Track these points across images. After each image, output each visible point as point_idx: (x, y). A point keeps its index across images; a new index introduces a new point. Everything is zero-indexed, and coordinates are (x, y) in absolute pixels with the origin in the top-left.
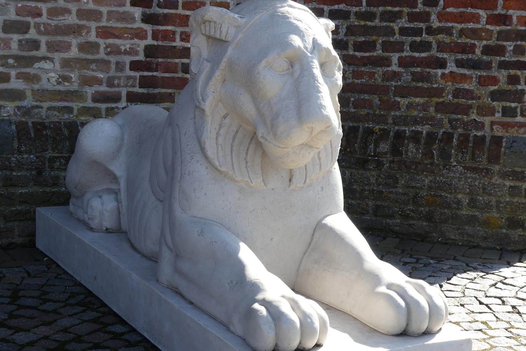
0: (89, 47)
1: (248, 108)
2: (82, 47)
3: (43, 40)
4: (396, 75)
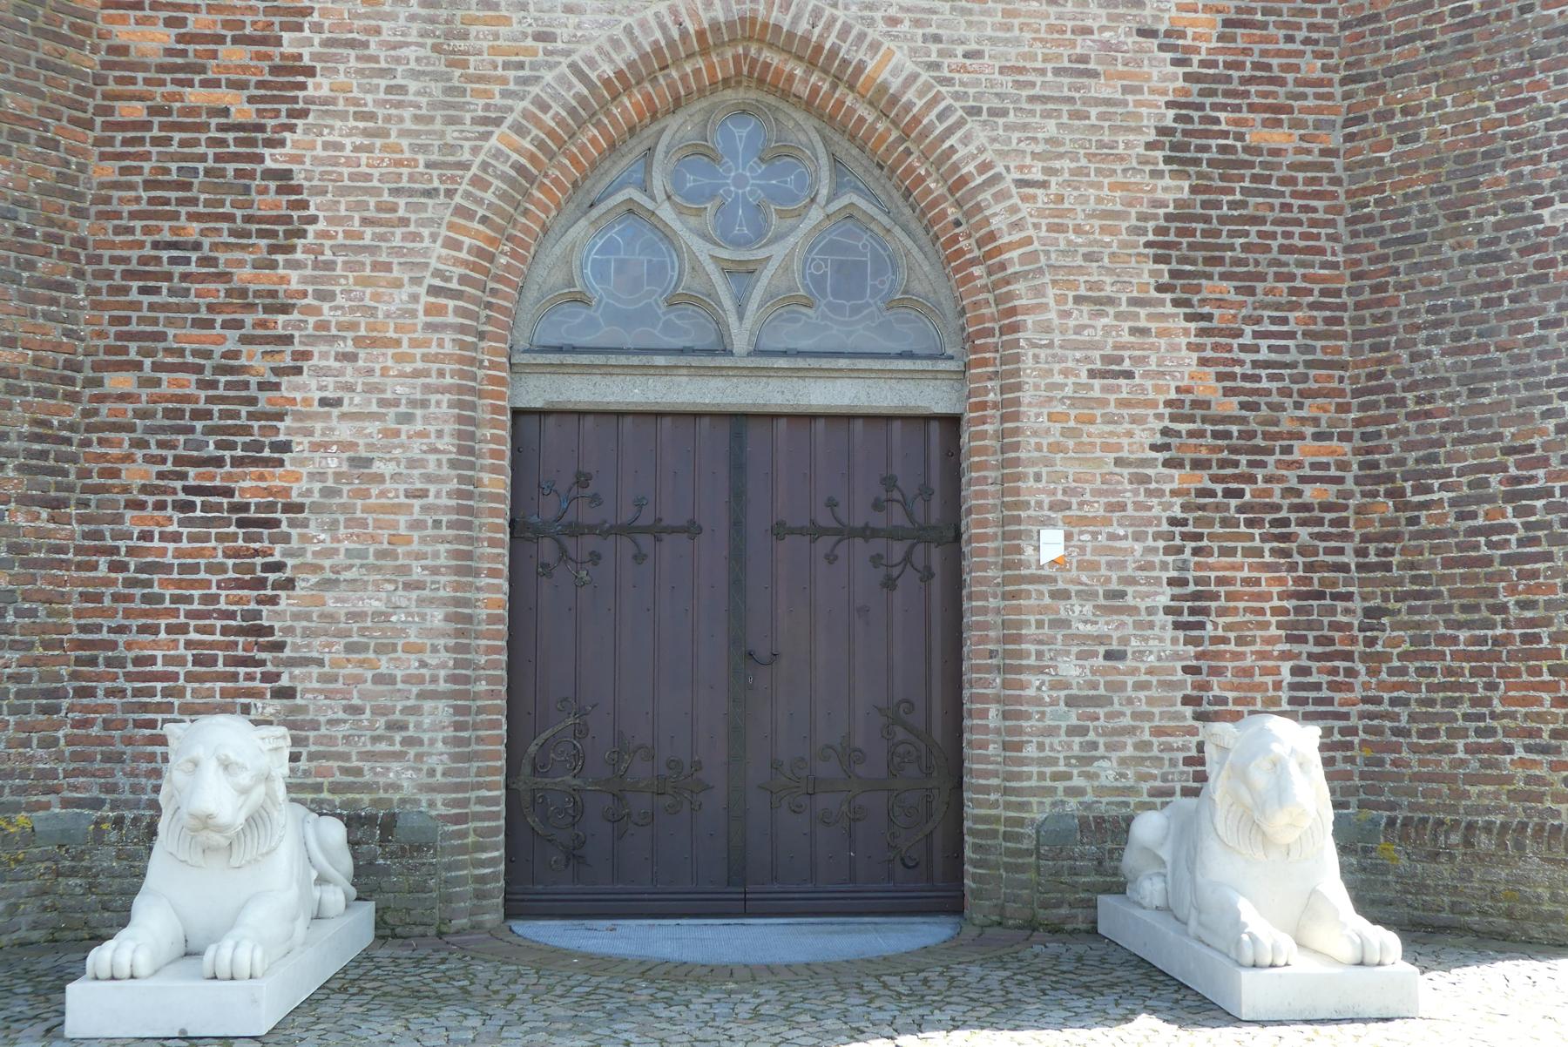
0: (1143, 746)
1: (1248, 799)
2: (1137, 746)
3: (1101, 741)
4: (1463, 762)
